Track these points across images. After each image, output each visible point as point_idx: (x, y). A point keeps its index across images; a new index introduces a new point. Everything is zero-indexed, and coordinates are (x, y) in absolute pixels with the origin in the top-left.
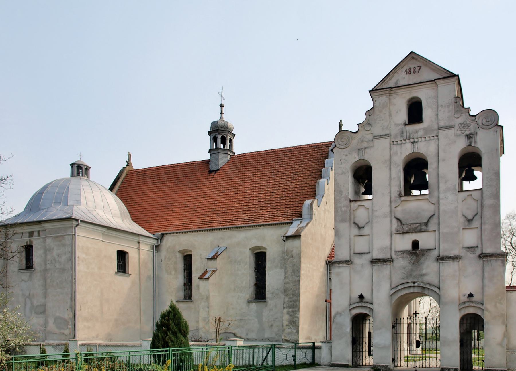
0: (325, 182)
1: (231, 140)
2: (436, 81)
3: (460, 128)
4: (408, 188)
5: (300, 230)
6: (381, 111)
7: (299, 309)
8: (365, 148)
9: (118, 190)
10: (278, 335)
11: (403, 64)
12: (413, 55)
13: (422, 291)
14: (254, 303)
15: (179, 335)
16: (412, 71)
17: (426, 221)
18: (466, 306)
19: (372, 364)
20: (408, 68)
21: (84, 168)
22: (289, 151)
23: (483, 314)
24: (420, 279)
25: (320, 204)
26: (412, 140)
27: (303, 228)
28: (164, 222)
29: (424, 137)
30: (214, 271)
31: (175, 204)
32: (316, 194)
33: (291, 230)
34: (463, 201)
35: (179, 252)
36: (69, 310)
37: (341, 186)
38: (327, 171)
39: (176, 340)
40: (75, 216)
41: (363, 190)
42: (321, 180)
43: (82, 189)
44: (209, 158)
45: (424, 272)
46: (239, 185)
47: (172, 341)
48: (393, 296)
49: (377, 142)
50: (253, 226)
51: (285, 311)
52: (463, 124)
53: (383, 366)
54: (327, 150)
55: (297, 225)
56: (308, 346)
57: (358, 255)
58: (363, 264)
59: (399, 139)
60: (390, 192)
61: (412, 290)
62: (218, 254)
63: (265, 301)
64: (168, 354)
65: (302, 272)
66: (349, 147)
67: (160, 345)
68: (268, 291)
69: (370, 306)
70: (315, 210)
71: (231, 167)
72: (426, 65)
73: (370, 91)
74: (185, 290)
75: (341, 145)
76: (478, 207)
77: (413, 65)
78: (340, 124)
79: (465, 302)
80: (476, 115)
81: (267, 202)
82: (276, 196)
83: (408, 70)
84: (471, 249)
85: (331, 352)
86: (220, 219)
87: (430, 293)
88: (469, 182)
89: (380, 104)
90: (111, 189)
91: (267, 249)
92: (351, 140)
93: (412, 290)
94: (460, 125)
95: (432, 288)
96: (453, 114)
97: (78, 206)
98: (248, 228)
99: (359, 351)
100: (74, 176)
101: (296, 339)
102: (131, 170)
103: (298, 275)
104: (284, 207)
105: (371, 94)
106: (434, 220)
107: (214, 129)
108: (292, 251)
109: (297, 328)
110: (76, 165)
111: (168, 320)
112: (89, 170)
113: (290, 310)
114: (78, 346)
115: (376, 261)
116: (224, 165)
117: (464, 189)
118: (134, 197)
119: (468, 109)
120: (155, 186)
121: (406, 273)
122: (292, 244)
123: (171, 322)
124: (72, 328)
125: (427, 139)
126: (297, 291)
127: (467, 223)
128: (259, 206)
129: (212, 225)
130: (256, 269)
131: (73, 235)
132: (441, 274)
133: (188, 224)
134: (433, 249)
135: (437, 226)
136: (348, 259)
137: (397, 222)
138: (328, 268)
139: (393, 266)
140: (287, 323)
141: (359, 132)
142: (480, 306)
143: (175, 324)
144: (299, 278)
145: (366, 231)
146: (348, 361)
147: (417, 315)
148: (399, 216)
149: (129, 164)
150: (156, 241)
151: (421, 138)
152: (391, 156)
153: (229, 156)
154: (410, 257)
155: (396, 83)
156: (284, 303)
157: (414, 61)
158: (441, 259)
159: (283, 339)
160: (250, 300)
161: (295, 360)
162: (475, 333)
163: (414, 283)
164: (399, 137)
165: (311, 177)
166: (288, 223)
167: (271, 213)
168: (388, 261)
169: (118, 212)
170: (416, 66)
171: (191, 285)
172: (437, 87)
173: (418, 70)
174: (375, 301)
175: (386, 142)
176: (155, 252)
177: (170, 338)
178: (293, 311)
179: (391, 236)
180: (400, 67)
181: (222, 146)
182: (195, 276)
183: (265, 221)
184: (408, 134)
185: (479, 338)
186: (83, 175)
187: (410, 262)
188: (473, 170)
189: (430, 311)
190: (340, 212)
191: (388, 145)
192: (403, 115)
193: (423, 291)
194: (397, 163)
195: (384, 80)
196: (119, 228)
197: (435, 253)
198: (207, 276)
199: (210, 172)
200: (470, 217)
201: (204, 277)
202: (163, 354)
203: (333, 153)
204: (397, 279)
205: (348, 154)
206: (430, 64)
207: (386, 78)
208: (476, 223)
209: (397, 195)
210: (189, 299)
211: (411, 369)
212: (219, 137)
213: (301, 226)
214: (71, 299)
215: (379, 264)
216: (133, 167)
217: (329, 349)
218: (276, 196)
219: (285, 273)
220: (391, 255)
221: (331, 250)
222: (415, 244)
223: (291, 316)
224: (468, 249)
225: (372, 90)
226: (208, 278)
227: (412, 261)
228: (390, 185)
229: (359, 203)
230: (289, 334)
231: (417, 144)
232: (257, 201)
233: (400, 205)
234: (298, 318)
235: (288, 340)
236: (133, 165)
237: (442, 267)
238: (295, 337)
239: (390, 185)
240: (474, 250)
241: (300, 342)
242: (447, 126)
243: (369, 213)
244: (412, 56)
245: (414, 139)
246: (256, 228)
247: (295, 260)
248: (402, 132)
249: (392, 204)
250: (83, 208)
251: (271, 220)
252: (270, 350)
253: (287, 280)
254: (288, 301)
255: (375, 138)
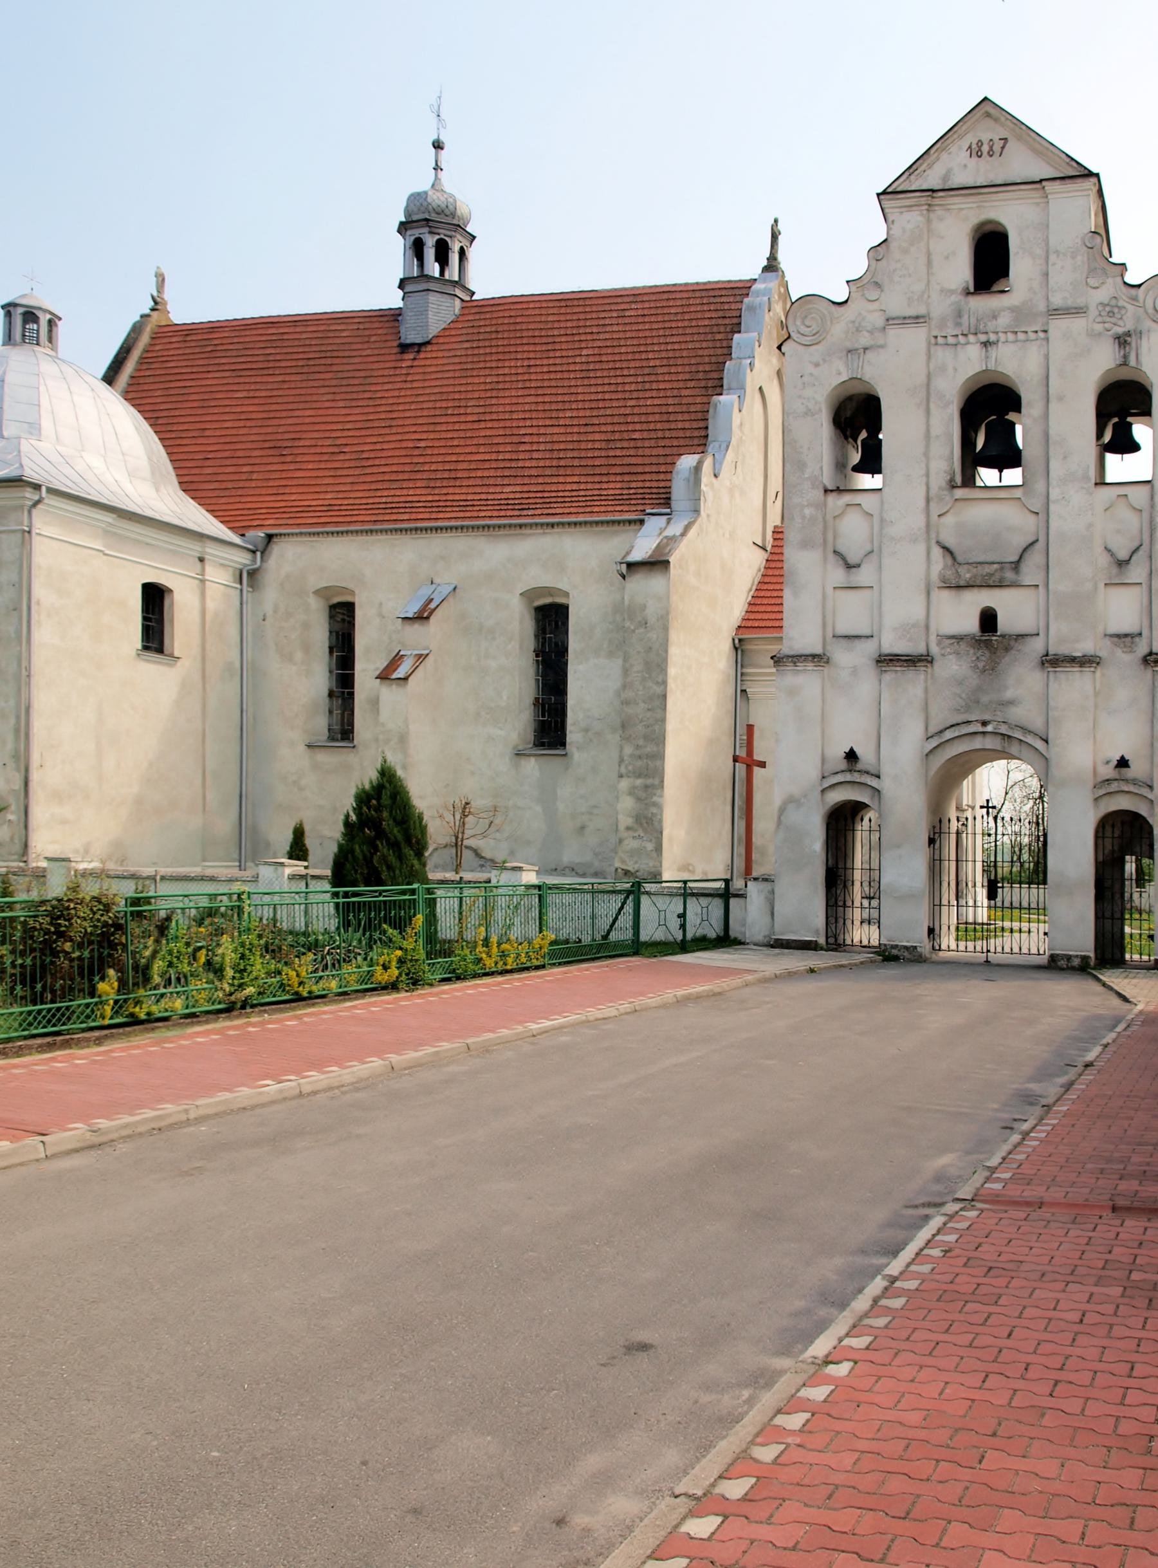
0: (732, 405)
1: (462, 253)
2: (1044, 183)
3: (1100, 315)
4: (971, 460)
5: (667, 545)
6: (905, 251)
7: (662, 781)
8: (865, 349)
9: (129, 385)
10: (600, 857)
11: (964, 128)
12: (986, 107)
13: (1004, 747)
14: (533, 759)
15: (409, 852)
16: (985, 148)
17: (1015, 558)
18: (1112, 790)
19: (876, 943)
20: (975, 142)
21: (44, 319)
22: (631, 299)
23: (1152, 815)
24: (999, 713)
25: (720, 470)
26: (983, 338)
27: (672, 539)
28: (272, 498)
29: (1013, 332)
30: (421, 658)
31: (301, 443)
32: (707, 436)
33: (643, 546)
34: (1106, 510)
35: (317, 592)
36: (11, 764)
37: (801, 447)
38: (739, 370)
39: (398, 864)
40: (30, 474)
41: (856, 457)
42: (721, 398)
43: (42, 388)
44: (400, 304)
45: (1009, 694)
46: (488, 395)
47: (390, 867)
48: (931, 757)
49: (892, 332)
50: (531, 525)
51: (624, 784)
52: (1108, 305)
53: (906, 948)
54: (738, 306)
55: (658, 531)
56: (712, 889)
57: (843, 641)
58: (855, 667)
59: (951, 331)
60: (927, 475)
61: (978, 743)
62: (432, 605)
63: (563, 753)
64: (415, 900)
65: (672, 671)
66: (823, 343)
67: (358, 876)
68: (574, 724)
69: (873, 782)
70: (706, 486)
71: (464, 338)
72: (1019, 138)
73: (878, 195)
74: (331, 712)
75: (803, 335)
76: (1141, 531)
77: (987, 133)
78: (772, 229)
79: (1108, 780)
80: (1139, 286)
81: (570, 454)
82: (597, 437)
83: (974, 146)
84: (1124, 639)
85: (773, 908)
86: (437, 498)
87: (1025, 751)
88: (1120, 456)
89: (904, 230)
90: (110, 378)
91: (571, 596)
92: (829, 323)
93: (978, 743)
94: (1100, 308)
95: (1029, 739)
96: (1084, 276)
97: (32, 442)
98: (518, 531)
99: (845, 906)
100: (15, 345)
101: (653, 870)
102: (164, 323)
103: (660, 680)
104: (618, 470)
105: (882, 203)
106: (1034, 559)
107: (415, 218)
108: (644, 607)
109: (657, 838)
110: (20, 310)
111: (378, 809)
112: (56, 325)
113: (639, 782)
114: (286, 876)
115: (891, 660)
116: (444, 329)
117: (1109, 479)
118: (177, 413)
119: (1119, 268)
120: (242, 380)
121: (964, 696)
122: (644, 585)
123: (385, 814)
124: (19, 820)
125: (1021, 336)
126: (657, 728)
127: (1115, 570)
128: (548, 463)
129: (414, 516)
130: (537, 656)
131: (24, 531)
132: (1052, 703)
133: (343, 508)
134: (1032, 635)
135: (1043, 574)
136: (818, 650)
137: (944, 557)
138: (739, 660)
139: (932, 675)
140: (629, 821)
141: (849, 302)
142: (1145, 791)
143: (395, 820)
144: (662, 687)
145: (864, 575)
146: (817, 932)
147: (990, 810)
148: (950, 542)
149: (157, 304)
150: (249, 556)
151: (1006, 333)
152: (929, 376)
153: (458, 302)
154: (975, 654)
155: (946, 178)
156: (621, 760)
157: (989, 123)
158: (1051, 662)
159: (617, 869)
160: (520, 748)
161: (683, 926)
162: (1130, 867)
163: (984, 724)
164: (950, 324)
165: (692, 384)
166: (634, 522)
167: (582, 487)
168: (920, 661)
169: (144, 463)
170: (996, 138)
171: (351, 695)
172: (1046, 200)
173: (1000, 150)
174: (886, 770)
175: (916, 337)
176: (248, 591)
177: (384, 858)
178: (646, 787)
179: (928, 593)
180: (955, 136)
181: (434, 269)
182: (364, 670)
183: (567, 511)
184: (973, 321)
185: (1142, 879)
186: (41, 342)
187: (976, 667)
188: (1130, 425)
189: (1006, 793)
190: (800, 521)
191: (923, 345)
192: (962, 270)
193: (1006, 745)
194: (944, 396)
195: (914, 167)
196: (148, 513)
197: (1037, 646)
198: (401, 672)
199: (404, 348)
200: (1123, 555)
201: (394, 676)
202: (364, 902)
203: (784, 354)
204: (941, 715)
205: (821, 362)
206: (1029, 135)
207: (920, 161)
208: (1137, 572)
209: (944, 484)
210: (343, 739)
211: (974, 957)
212: (430, 242)
213: (670, 532)
214: (17, 730)
215: (898, 669)
216: (170, 315)
217: (766, 898)
218: (597, 437)
219: (626, 671)
220: (927, 646)
221: (747, 605)
222: (988, 619)
223: (639, 799)
224: (1116, 639)
225: (884, 193)
226: (406, 679)
227: (981, 665)
228: (926, 455)
229: (847, 498)
230: (635, 853)
231: (994, 347)
232: (542, 447)
233: (951, 511)
234: (659, 806)
235: (633, 871)
236: (169, 308)
237: (1053, 686)
238: (651, 864)
239: (926, 455)
240: (1132, 643)
241: (664, 879)
242: (1068, 309)
243: (872, 528)
244: (985, 108)
245: (987, 333)
246: (542, 531)
247: (653, 635)
248: (959, 314)
249: (932, 504)
250: (45, 446)
251: (582, 510)
252: (627, 897)
253: (629, 694)
254: (631, 756)
255: (891, 322)
